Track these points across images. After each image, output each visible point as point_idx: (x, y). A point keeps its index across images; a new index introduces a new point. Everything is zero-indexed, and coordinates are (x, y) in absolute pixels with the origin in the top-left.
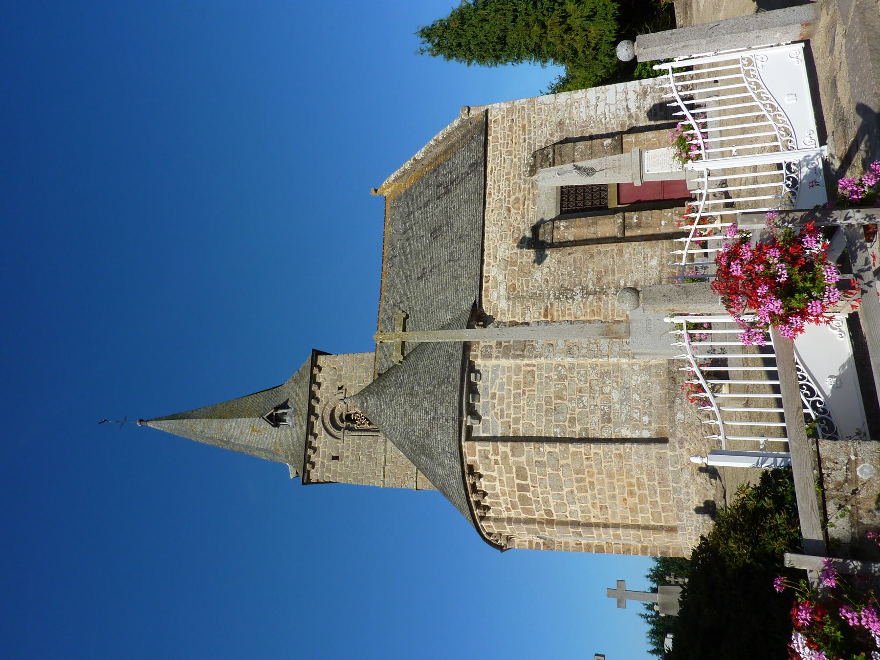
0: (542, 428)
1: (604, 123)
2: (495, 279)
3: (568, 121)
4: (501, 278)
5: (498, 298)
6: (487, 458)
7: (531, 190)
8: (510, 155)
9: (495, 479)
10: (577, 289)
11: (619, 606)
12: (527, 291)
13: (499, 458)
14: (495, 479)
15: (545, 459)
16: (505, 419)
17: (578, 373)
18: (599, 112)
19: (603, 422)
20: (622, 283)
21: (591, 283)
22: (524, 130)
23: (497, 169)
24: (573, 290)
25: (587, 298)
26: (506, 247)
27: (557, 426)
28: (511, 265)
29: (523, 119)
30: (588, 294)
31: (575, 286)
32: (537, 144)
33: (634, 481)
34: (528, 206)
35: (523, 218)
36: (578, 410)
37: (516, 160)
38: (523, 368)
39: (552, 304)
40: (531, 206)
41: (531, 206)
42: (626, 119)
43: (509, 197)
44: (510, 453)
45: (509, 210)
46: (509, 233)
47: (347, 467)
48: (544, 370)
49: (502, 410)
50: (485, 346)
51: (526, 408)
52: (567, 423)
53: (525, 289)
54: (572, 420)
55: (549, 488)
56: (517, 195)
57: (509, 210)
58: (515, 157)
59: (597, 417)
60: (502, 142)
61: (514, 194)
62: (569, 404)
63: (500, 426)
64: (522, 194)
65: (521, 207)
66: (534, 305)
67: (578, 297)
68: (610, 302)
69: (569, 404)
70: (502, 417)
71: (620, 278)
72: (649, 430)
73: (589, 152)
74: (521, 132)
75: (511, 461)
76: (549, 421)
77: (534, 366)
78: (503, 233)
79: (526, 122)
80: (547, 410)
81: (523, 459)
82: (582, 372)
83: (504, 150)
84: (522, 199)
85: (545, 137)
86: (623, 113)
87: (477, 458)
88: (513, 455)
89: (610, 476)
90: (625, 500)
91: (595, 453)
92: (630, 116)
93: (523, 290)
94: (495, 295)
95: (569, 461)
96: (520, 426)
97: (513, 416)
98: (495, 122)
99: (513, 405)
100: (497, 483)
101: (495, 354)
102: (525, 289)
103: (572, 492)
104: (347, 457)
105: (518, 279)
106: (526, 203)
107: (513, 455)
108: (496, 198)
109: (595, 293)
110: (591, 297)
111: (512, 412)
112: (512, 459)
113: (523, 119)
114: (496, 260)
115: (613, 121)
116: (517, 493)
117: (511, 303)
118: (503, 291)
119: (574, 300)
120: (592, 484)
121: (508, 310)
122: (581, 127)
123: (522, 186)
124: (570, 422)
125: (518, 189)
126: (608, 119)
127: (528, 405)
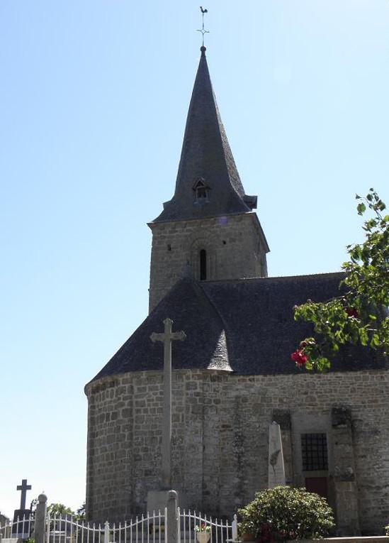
0: (141, 430)
1: (375, 467)
2: (252, 386)
3: (378, 437)
4: (252, 390)
5: (237, 390)
6: (122, 393)
7: (321, 410)
8: (351, 392)
9: (112, 397)
10: (242, 449)
11: (18, 487)
12: (242, 411)
13: (122, 400)
14: (112, 397)
15: (121, 432)
16: (146, 403)
17: (177, 453)
18: (384, 462)
19: (146, 471)
20: (246, 482)
21: (247, 459)
22: (372, 401)
23: (340, 382)
24: (242, 445)
25: (236, 456)
26: (276, 393)
27: (142, 439)
28: (262, 398)
29: (382, 401)
30: (239, 457)
31: (245, 447)
32: (360, 413)
33: (112, 492)
34: (308, 408)
35: (299, 405)
36: (153, 453)
37: (347, 397)
38: (181, 413)
39: (232, 430)
40: (308, 410)
41: (308, 410)
42: (377, 485)
43: (317, 393)
44: (124, 408)
45: (306, 393)
46: (287, 395)
47: (163, 258)
48: (180, 428)
49: (153, 400)
50: (196, 384)
51: (154, 417)
52: (144, 446)
53: (244, 410)
54: (146, 450)
55: (108, 434)
56: (317, 399)
57: (306, 393)
58: (349, 396)
59: (148, 466)
60: (364, 384)
61: (319, 397)
62: (157, 447)
63: (142, 399)
64: (319, 403)
65: (307, 403)
66: (232, 417)
67: (236, 450)
68: (233, 473)
69: (157, 447)
70: (148, 400)
71: (249, 480)
72: (140, 502)
73: (344, 456)
74: (371, 399)
75: (119, 409)
76: (145, 433)
77: (183, 421)
78: (287, 390)
79: (380, 403)
80: (153, 432)
81: (121, 417)
82: (178, 456)
83: (356, 386)
84: (314, 403)
85: (365, 419)
86: (383, 482)
87: (121, 385)
88: (123, 410)
89: (115, 476)
90: (103, 486)
91: (124, 466)
92: (379, 488)
93: (242, 408)
94: (240, 387)
95: (120, 449)
96: (142, 414)
97: (149, 408)
98: (382, 377)
99: (156, 407)
100: (109, 399)
101: (189, 392)
102: (244, 410)
103: (106, 450)
104: (170, 257)
105: (136, 439)
106: (311, 407)
107: (123, 410)
108: (315, 382)
109: (239, 462)
110: (236, 459)
111: (152, 407)
112: (121, 409)
113: (382, 401)
114: (188, 411)
115: (376, 474)
116: (105, 413)
117: (234, 399)
118: (244, 392)
119: (235, 447)
120: (110, 464)
121: (228, 398)
122: (372, 449)
123: (325, 403)
124: (145, 448)
125: (322, 399)
126: (377, 470)
127: (156, 418)
